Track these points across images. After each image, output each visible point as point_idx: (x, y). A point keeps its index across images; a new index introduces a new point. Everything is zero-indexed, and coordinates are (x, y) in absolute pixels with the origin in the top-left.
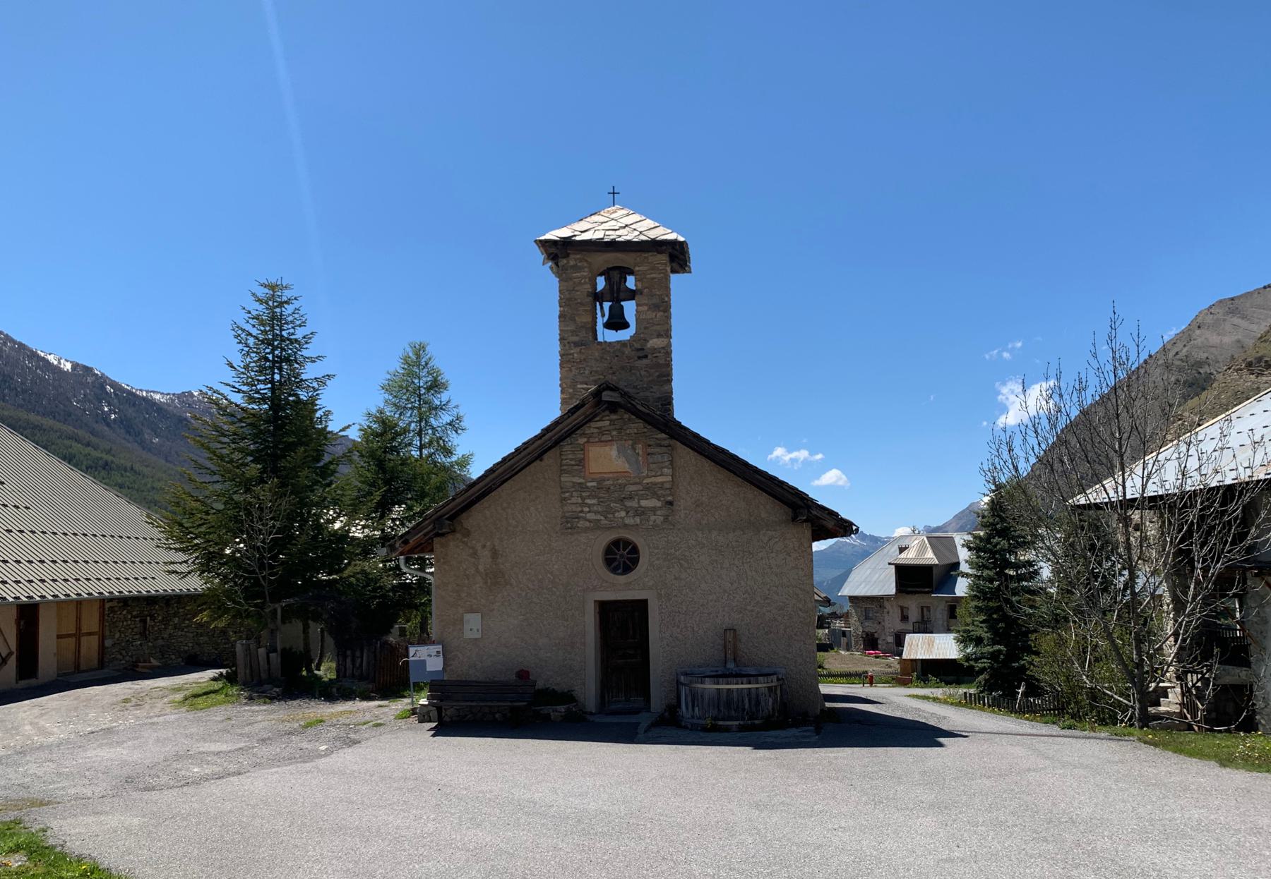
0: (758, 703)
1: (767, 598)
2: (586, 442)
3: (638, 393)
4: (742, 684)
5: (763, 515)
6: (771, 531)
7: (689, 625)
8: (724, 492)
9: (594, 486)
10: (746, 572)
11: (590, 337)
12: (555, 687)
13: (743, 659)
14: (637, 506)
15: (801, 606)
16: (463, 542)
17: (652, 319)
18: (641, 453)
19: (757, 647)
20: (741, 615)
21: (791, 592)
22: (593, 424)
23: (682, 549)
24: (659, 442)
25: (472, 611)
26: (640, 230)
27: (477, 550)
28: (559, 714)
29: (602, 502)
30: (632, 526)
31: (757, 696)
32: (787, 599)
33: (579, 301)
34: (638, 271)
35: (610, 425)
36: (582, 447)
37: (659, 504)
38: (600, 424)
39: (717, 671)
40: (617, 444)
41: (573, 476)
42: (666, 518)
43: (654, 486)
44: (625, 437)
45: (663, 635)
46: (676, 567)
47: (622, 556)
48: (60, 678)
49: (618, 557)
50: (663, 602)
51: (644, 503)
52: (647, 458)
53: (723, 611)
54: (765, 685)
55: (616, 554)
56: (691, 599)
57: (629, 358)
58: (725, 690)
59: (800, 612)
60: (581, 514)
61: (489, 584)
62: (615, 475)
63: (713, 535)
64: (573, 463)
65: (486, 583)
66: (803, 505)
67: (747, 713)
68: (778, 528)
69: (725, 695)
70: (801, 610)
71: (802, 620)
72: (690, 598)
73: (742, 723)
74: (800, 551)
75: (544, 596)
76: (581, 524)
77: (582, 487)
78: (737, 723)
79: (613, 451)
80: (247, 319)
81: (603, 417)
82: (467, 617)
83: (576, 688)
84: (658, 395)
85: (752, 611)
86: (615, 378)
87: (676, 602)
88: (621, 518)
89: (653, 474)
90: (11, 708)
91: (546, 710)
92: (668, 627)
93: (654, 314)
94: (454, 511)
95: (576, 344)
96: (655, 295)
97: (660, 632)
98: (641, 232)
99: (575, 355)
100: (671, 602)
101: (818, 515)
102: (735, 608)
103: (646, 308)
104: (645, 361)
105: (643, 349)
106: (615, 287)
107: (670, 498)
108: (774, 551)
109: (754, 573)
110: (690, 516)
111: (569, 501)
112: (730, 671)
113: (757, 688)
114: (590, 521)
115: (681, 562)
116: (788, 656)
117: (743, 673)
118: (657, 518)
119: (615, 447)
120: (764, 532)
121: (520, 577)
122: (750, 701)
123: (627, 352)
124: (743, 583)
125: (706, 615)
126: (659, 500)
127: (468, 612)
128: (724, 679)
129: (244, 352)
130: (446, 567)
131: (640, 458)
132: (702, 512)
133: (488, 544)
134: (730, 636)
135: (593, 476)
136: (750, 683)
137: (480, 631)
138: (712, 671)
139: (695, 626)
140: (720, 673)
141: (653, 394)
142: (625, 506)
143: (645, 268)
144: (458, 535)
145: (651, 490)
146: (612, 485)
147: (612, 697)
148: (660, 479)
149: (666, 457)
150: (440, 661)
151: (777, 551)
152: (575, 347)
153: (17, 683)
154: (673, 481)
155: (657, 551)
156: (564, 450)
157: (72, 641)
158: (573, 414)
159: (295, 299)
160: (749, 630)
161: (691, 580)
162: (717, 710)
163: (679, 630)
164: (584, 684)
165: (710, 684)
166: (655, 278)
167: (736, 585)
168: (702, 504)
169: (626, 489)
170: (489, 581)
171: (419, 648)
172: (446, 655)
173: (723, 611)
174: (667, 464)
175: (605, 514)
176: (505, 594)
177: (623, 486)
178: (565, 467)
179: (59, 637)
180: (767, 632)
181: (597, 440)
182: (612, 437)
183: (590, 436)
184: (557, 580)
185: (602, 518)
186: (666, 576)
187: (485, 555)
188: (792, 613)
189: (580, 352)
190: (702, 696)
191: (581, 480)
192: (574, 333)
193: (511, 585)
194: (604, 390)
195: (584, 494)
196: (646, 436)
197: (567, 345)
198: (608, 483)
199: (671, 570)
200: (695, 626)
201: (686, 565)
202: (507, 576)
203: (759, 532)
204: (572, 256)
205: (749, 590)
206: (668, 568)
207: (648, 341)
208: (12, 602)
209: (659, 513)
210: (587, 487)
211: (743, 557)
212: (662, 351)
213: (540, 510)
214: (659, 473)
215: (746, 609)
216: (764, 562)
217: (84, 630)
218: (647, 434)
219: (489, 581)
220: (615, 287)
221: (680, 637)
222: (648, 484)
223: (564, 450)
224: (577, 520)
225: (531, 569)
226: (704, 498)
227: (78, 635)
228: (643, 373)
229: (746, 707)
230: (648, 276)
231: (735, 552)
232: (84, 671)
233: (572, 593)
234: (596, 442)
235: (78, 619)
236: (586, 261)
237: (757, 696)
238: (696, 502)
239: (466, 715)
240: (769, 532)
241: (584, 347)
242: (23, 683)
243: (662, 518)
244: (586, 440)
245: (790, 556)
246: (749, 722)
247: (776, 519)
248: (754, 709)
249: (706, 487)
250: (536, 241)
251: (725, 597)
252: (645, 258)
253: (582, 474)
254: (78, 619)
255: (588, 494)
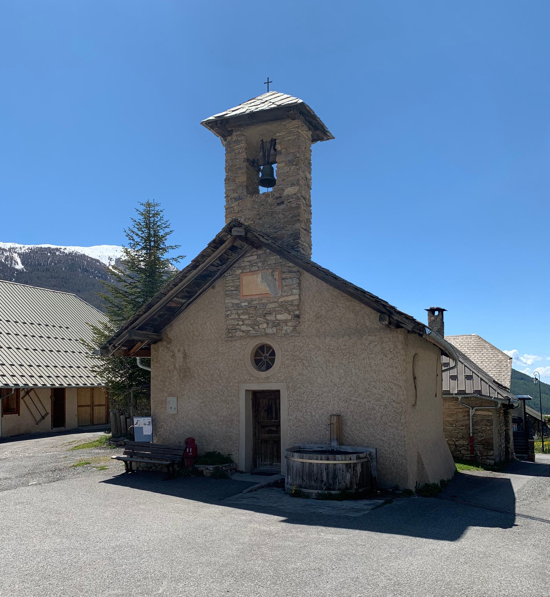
0: (335, 476)
1: (367, 391)
2: (241, 273)
3: (277, 232)
4: (321, 460)
5: (368, 323)
6: (371, 336)
7: (308, 410)
8: (338, 306)
9: (246, 306)
10: (351, 370)
11: (245, 193)
12: (220, 451)
13: (348, 439)
14: (274, 319)
15: (394, 398)
16: (167, 348)
17: (287, 172)
18: (277, 278)
19: (358, 430)
20: (347, 404)
21: (387, 386)
22: (246, 259)
23: (305, 352)
24: (290, 269)
25: (171, 395)
26: (273, 102)
27: (175, 353)
28: (209, 471)
29: (251, 317)
30: (271, 334)
31: (335, 470)
32: (384, 392)
33: (238, 166)
34: (279, 136)
35: (257, 258)
36: (239, 276)
37: (289, 317)
38: (251, 258)
39: (322, 447)
40: (261, 273)
41: (233, 299)
42: (295, 327)
43: (286, 304)
44: (267, 267)
45: (291, 417)
46: (300, 365)
47: (266, 357)
48: (79, 428)
49: (263, 358)
50: (290, 392)
51: (279, 317)
52: (282, 282)
53: (334, 400)
54: (343, 462)
55: (262, 356)
56: (310, 391)
57: (271, 205)
58: (308, 464)
59: (393, 403)
60: (238, 327)
61: (181, 377)
62: (260, 296)
63: (327, 341)
64: (233, 289)
65: (180, 376)
66: (386, 311)
67: (325, 484)
68: (378, 333)
69: (307, 468)
70: (394, 401)
71: (395, 409)
72: (310, 389)
73: (320, 492)
74: (395, 352)
75: (214, 386)
76: (239, 334)
77: (238, 306)
78: (316, 491)
79: (258, 278)
80: (134, 225)
81: (253, 253)
82: (170, 399)
83: (233, 453)
84: (291, 232)
85: (355, 401)
86: (261, 222)
87: (300, 393)
88: (264, 329)
89: (286, 294)
90: (27, 442)
91: (201, 467)
92: (294, 411)
93: (289, 168)
94: (142, 324)
95: (236, 199)
96: (290, 153)
97: (288, 415)
98: (273, 103)
99: (235, 208)
100: (296, 392)
101: (399, 320)
102: (343, 399)
103: (284, 164)
104: (282, 207)
105: (281, 197)
106: (267, 153)
107: (297, 313)
108: (374, 353)
109: (357, 370)
110: (312, 326)
111: (229, 317)
112: (332, 448)
113: (335, 464)
114: (243, 332)
115: (304, 361)
116: (383, 439)
117: (342, 450)
118: (288, 328)
119: (260, 275)
120: (366, 337)
121: (200, 372)
122: (327, 474)
123: (269, 201)
124: (349, 379)
125: (321, 403)
126: (289, 314)
127: (169, 396)
128: (307, 455)
129: (132, 245)
130: (157, 364)
131: (277, 283)
132: (321, 322)
133: (182, 348)
134: (334, 420)
135: (246, 298)
136: (328, 460)
137: (176, 409)
138: (318, 447)
139: (313, 411)
140: (324, 449)
141: (287, 232)
142: (267, 320)
143: (283, 133)
144: (165, 343)
145: (284, 307)
146: (258, 304)
147: (262, 462)
148: (291, 298)
149: (295, 280)
150: (150, 427)
151: (376, 352)
152: (235, 201)
153: (52, 429)
154: (300, 299)
155: (287, 353)
156: (227, 279)
157: (89, 409)
158: (217, 248)
159: (161, 211)
160: (353, 416)
161: (310, 375)
162: (301, 480)
163: (301, 414)
164: (238, 450)
165: (297, 458)
166: (290, 140)
167: (343, 380)
168: (321, 316)
169: (267, 307)
170: (182, 374)
171: (139, 419)
172: (154, 424)
173: (334, 400)
174: (295, 286)
175: (252, 326)
176: (191, 384)
177: (265, 305)
178: (228, 292)
179: (79, 406)
180: (367, 418)
181: (248, 270)
182: (258, 268)
183: (244, 268)
184: (222, 375)
185: (251, 329)
186: (293, 372)
187: (180, 356)
188: (387, 403)
189: (238, 205)
190: (292, 467)
191: (238, 302)
192: (234, 190)
193: (195, 378)
194: (235, 226)
195: (239, 312)
196: (281, 265)
197: (230, 201)
198: (255, 302)
199: (297, 367)
200: (313, 411)
201: (307, 364)
202: (192, 371)
203: (362, 337)
204: (234, 134)
205: (354, 385)
206: (295, 366)
207: (284, 190)
208: (22, 386)
209: (289, 324)
210: (242, 307)
211: (349, 358)
212: (294, 197)
213: (213, 324)
214: (289, 294)
215: (351, 400)
216: (365, 362)
217: (96, 403)
218: (282, 264)
219: (182, 374)
220: (267, 153)
221: (303, 419)
222: (282, 302)
223: (227, 279)
224: (235, 331)
225: (206, 367)
226: (323, 312)
227: (92, 406)
228: (280, 216)
229: (324, 480)
230: (285, 139)
231: (344, 354)
232: (96, 425)
233: (231, 384)
234: (248, 272)
235: (92, 397)
236: (243, 135)
237: (335, 470)
238: (316, 315)
239: (151, 467)
240: (370, 337)
241: (240, 201)
242: (55, 430)
243: (291, 328)
244: (241, 271)
245: (386, 356)
246: (326, 492)
247: (378, 327)
248: (331, 482)
249: (325, 303)
250: (202, 123)
251: (335, 390)
252: (285, 125)
253: (238, 297)
254: (92, 397)
255: (242, 311)
